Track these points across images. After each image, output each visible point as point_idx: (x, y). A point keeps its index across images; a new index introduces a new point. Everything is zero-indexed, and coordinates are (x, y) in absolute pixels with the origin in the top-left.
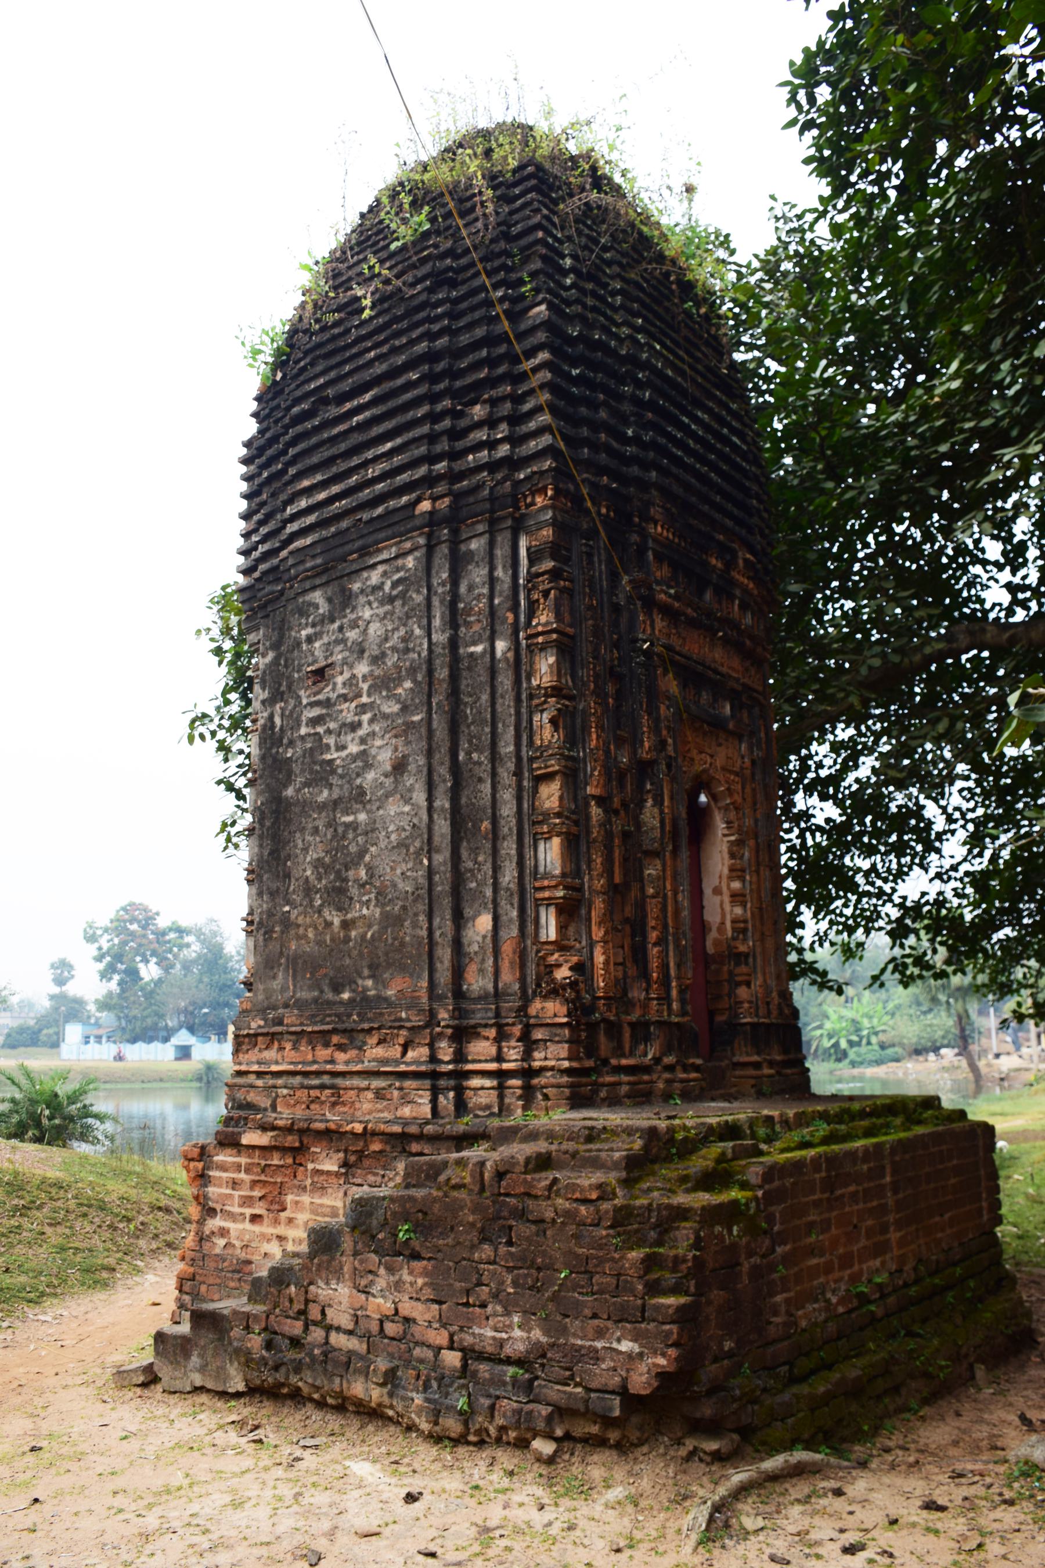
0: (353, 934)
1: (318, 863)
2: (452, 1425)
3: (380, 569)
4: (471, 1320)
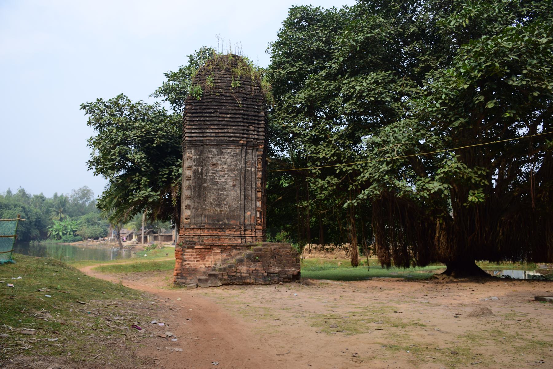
1: (214, 199)
2: (268, 282)
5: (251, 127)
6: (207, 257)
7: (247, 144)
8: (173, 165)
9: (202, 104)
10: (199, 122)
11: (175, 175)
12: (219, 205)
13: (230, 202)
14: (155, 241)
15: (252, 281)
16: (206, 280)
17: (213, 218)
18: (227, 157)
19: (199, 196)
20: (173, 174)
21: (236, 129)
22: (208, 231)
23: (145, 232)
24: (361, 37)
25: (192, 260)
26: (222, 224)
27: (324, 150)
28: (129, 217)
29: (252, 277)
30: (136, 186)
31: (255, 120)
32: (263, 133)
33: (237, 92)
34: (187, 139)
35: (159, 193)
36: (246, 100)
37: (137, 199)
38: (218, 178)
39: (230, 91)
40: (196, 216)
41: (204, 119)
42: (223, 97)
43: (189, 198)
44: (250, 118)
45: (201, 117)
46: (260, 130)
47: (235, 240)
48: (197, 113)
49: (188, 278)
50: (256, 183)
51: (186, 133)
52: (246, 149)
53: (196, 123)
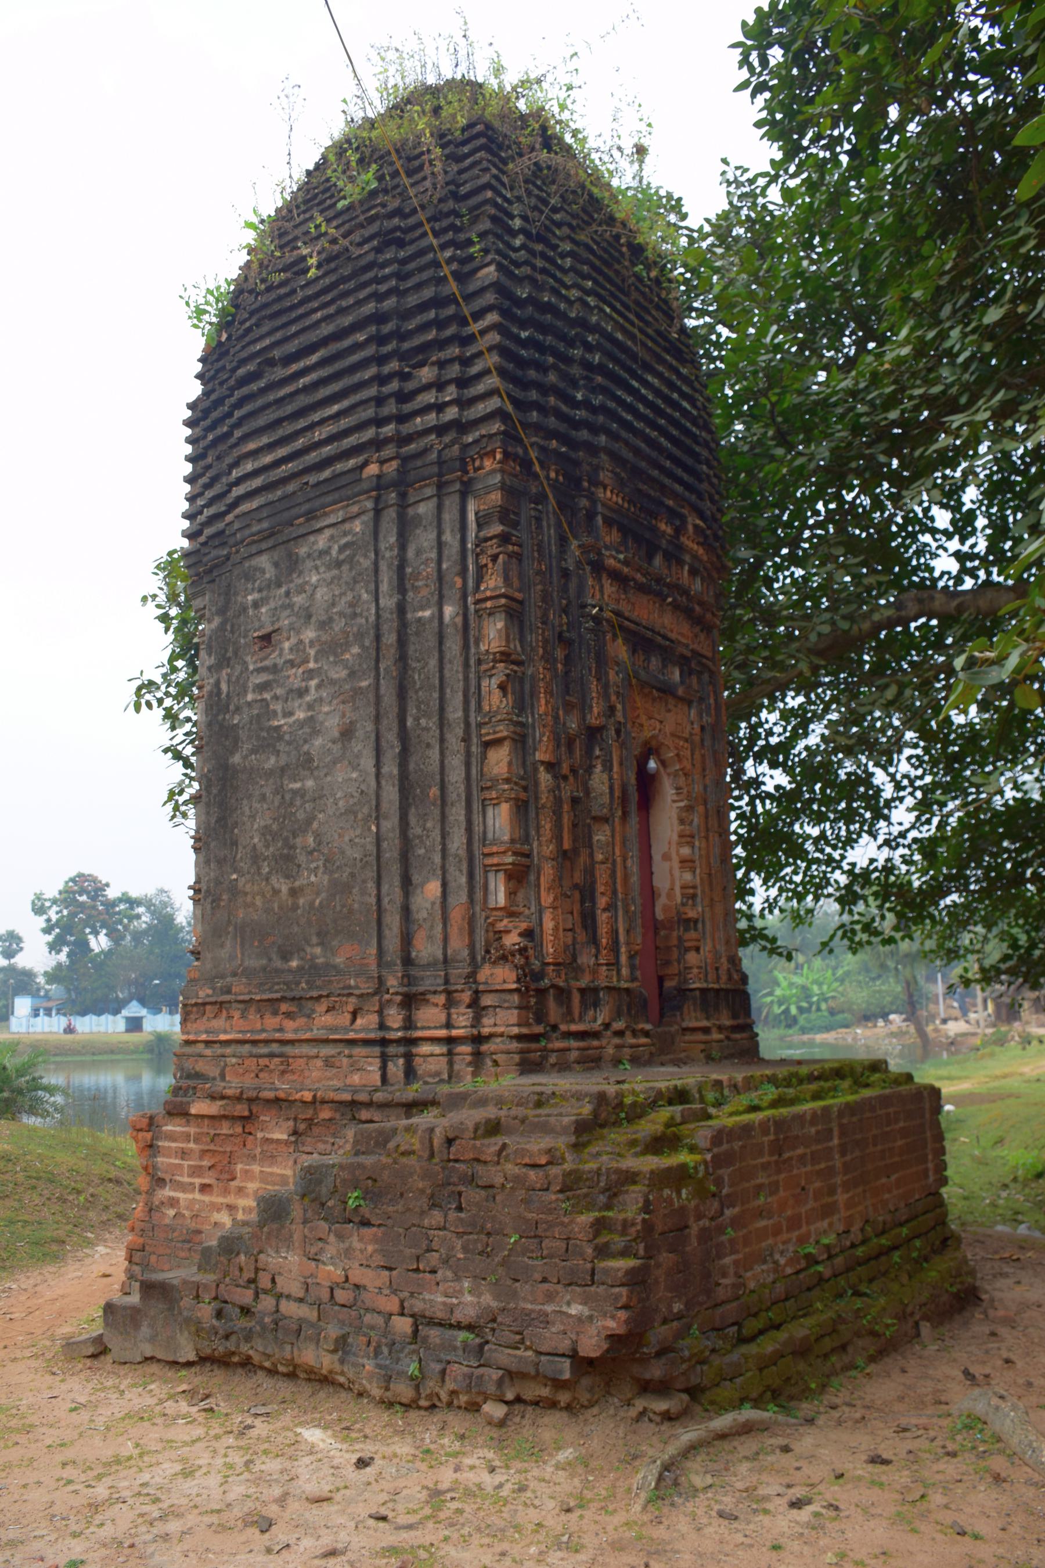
0: (301, 901)
1: (265, 831)
3: (327, 533)
7: (402, 471)
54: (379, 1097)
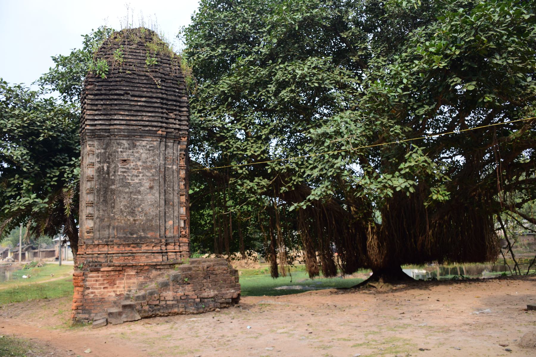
0: (137, 222)
1: (125, 206)
2: (201, 310)
3: (146, 142)
4: (202, 293)
5: (171, 114)
6: (117, 282)
7: (166, 135)
8: (65, 164)
9: (108, 84)
10: (104, 107)
11: (68, 177)
12: (133, 213)
13: (147, 209)
14: (35, 258)
15: (181, 310)
16: (120, 314)
17: (124, 230)
18: (141, 151)
19: (105, 201)
20: (65, 176)
21: (152, 116)
22: (118, 247)
23: (22, 249)
24: (299, 16)
25: (97, 287)
26: (137, 238)
27: (252, 147)
28: (4, 233)
29: (180, 305)
30: (15, 191)
31: (176, 106)
32: (185, 123)
33: (153, 71)
34: (88, 127)
35: (46, 200)
36: (164, 81)
37: (16, 208)
38: (129, 178)
39: (144, 70)
40: (102, 228)
41: (111, 102)
42: (135, 76)
43: (91, 204)
44: (170, 103)
45: (107, 100)
46: (182, 119)
47: (155, 258)
48: (101, 95)
49: (93, 311)
50: (179, 185)
51: (86, 120)
52: (166, 142)
53: (99, 107)
54: (162, 263)
